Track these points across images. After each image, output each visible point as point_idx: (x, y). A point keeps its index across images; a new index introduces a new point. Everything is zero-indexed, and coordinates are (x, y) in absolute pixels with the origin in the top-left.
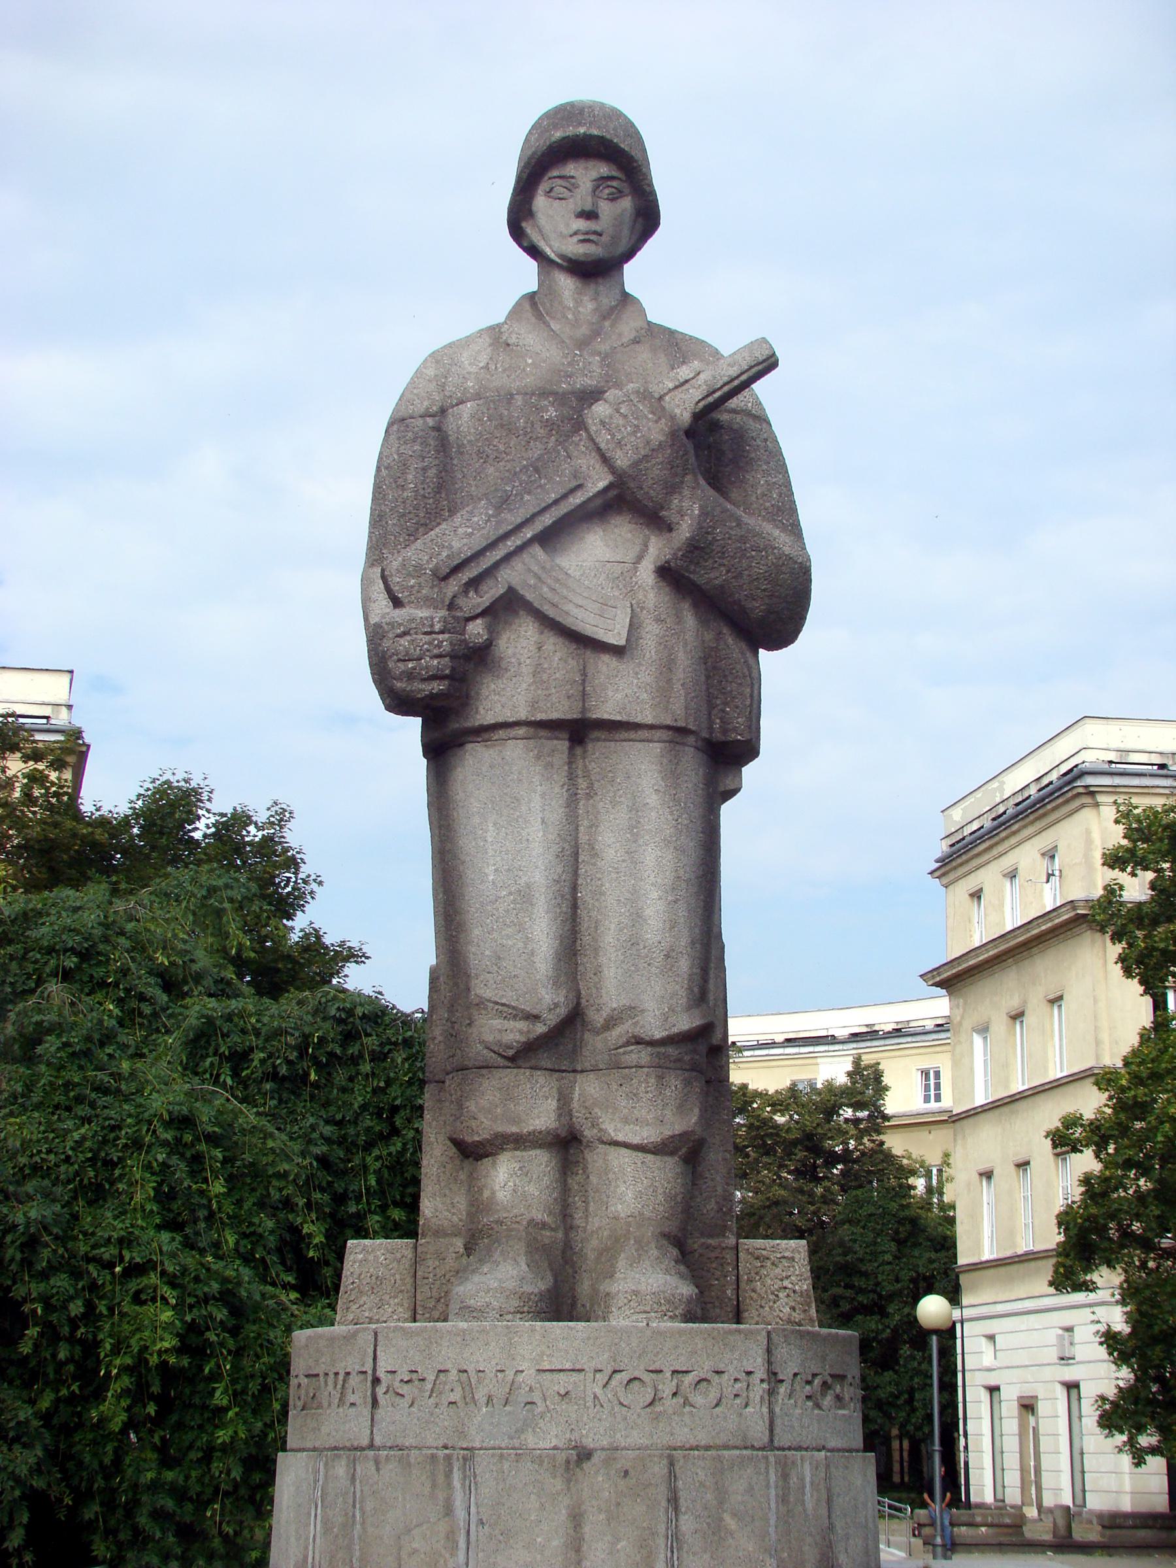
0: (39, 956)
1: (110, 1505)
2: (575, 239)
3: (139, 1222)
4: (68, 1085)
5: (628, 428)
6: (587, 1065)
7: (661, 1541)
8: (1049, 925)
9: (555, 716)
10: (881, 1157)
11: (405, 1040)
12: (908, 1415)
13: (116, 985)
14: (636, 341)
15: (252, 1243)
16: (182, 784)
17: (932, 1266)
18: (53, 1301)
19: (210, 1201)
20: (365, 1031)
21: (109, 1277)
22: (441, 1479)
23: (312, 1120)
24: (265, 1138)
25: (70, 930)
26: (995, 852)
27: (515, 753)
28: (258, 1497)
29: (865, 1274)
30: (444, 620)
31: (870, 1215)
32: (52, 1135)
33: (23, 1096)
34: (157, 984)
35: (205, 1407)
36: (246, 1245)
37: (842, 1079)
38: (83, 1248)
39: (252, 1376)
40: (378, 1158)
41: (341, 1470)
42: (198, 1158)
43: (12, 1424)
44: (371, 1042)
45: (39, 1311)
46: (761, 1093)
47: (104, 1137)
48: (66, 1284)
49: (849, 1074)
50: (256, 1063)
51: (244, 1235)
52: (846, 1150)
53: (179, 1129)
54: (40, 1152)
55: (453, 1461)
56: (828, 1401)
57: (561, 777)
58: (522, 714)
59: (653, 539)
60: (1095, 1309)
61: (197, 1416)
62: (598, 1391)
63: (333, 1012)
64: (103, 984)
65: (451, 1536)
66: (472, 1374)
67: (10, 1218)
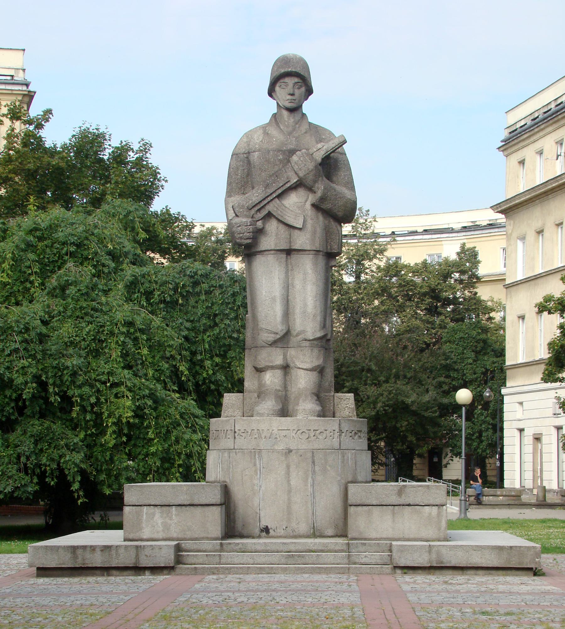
0: (58, 246)
1: (109, 475)
2: (288, 101)
3: (115, 365)
4: (81, 308)
5: (302, 165)
6: (291, 346)
7: (310, 472)
8: (557, 184)
9: (282, 248)
10: (475, 301)
11: (220, 285)
12: (479, 444)
13: (93, 259)
14: (306, 133)
15: (159, 373)
16: (95, 131)
17: (494, 365)
18: (84, 397)
19: (142, 356)
20: (202, 281)
21: (105, 388)
22: (253, 457)
23: (181, 321)
24: (163, 330)
25: (72, 235)
26: (532, 139)
27: (271, 258)
28: (167, 473)
29: (457, 370)
30: (250, 222)
31: (461, 338)
32: (77, 329)
33: (63, 312)
34: (110, 259)
35: (144, 439)
36: (157, 374)
37: (453, 257)
38: (93, 376)
39: (163, 427)
40: (208, 337)
41: (226, 455)
42: (136, 339)
43: (72, 444)
44: (205, 286)
45: (79, 401)
46: (406, 266)
47: (98, 330)
48: (88, 390)
49: (458, 254)
50: (156, 296)
51: (156, 370)
52: (455, 298)
53: (128, 327)
54: (73, 336)
55: (256, 453)
56: (356, 437)
57: (284, 265)
58: (273, 247)
59: (310, 195)
60: (557, 391)
61: (141, 442)
62: (294, 435)
63: (188, 273)
64: (87, 259)
65: (256, 471)
66: (261, 430)
67: (66, 364)
